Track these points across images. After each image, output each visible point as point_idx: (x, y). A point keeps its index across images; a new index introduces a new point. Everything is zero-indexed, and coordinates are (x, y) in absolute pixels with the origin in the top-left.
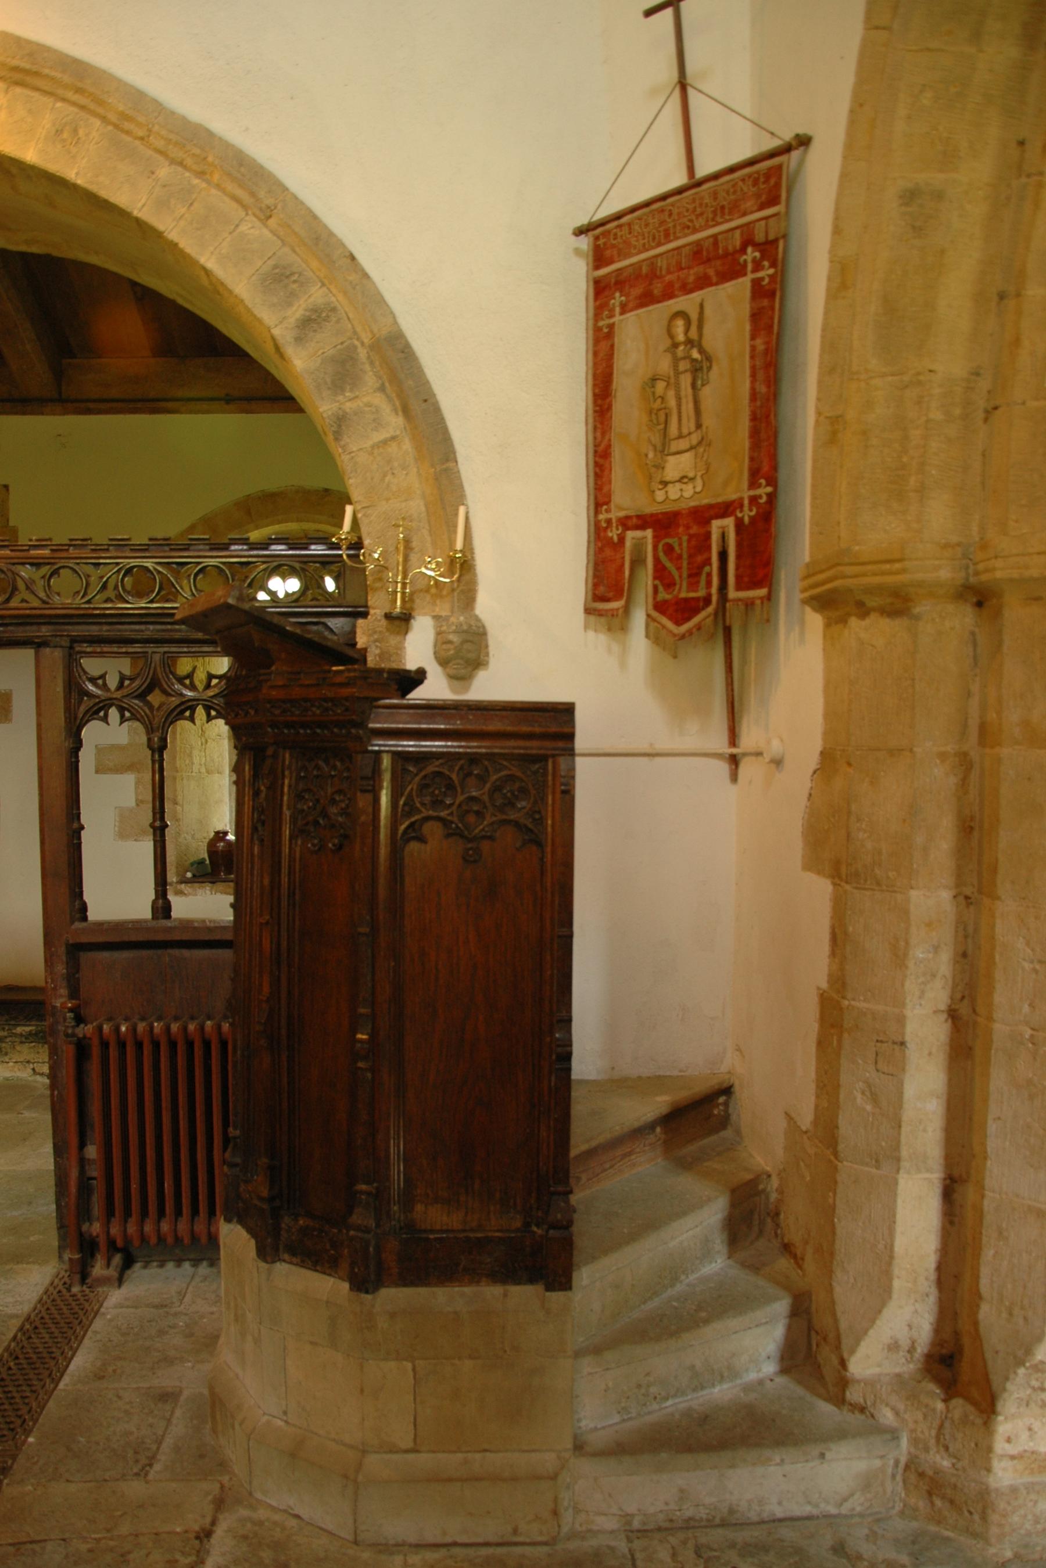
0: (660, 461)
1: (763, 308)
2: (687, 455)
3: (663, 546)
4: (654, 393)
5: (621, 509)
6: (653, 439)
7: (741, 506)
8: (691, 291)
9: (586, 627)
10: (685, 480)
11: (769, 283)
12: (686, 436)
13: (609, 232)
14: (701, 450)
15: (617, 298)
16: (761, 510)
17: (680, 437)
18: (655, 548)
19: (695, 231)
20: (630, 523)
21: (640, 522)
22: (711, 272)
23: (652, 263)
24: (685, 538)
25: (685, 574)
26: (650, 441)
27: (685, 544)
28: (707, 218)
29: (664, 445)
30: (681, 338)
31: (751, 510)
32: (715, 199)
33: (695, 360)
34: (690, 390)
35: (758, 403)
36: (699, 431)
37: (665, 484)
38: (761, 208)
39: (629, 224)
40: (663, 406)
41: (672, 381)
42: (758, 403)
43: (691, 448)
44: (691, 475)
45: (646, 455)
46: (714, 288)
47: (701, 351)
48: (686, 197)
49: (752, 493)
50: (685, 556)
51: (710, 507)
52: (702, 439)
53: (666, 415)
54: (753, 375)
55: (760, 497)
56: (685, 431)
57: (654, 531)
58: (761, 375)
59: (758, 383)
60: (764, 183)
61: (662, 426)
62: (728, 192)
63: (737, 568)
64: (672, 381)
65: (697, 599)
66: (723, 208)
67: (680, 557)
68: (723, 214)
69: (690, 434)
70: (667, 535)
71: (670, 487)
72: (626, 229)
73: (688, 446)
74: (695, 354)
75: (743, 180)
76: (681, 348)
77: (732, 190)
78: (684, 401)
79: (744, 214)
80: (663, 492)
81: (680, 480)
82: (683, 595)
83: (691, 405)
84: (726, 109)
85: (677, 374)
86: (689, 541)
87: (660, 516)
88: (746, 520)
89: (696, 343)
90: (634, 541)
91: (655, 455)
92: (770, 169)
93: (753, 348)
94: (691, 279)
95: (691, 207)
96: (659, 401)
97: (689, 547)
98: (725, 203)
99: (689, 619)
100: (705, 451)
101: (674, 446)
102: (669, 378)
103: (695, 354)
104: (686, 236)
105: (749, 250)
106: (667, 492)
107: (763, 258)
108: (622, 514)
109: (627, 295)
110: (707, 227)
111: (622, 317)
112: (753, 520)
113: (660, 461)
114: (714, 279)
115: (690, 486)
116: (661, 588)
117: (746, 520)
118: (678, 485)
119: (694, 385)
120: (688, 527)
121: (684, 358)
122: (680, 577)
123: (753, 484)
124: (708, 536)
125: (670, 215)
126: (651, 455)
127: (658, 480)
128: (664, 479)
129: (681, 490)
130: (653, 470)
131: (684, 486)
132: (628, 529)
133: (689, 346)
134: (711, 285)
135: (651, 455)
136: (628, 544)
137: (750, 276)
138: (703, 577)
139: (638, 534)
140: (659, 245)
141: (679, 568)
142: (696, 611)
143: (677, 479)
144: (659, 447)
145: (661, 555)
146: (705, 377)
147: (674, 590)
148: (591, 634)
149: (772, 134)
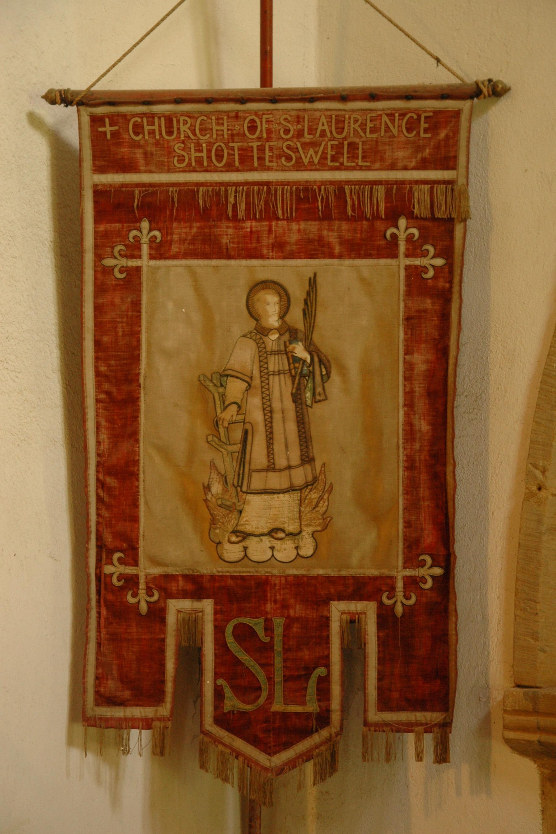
0: (235, 500)
1: (425, 311)
2: (285, 498)
3: (235, 627)
4: (223, 396)
5: (154, 561)
6: (219, 463)
7: (392, 589)
8: (292, 256)
9: (70, 742)
10: (281, 535)
11: (434, 278)
12: (281, 470)
13: (125, 117)
14: (314, 496)
15: (145, 232)
16: (424, 600)
17: (271, 468)
18: (219, 630)
19: (299, 166)
20: (173, 587)
21: (189, 587)
22: (332, 237)
23: (218, 194)
24: (279, 622)
25: (278, 677)
26: (213, 466)
27: (279, 631)
28: (324, 153)
29: (240, 476)
30: (273, 321)
31: (408, 598)
32: (340, 130)
33: (296, 360)
34: (290, 405)
35: (417, 446)
36: (308, 467)
37: (245, 536)
38: (423, 165)
39: (169, 119)
40: (240, 417)
41: (257, 382)
42: (417, 446)
43: (291, 489)
44: (291, 528)
45: (207, 488)
46: (335, 261)
47: (311, 348)
48: (287, 111)
49: (409, 572)
50: (278, 647)
51: (330, 580)
52: (315, 479)
53: (246, 433)
54: (410, 404)
55: (423, 580)
56: (281, 462)
57: (216, 604)
58: (421, 405)
59: (417, 416)
60: (426, 131)
61: (237, 448)
62: (363, 126)
63: (381, 678)
64: (257, 382)
65: (308, 716)
66: (353, 146)
67: (269, 647)
68: (353, 156)
69: (289, 467)
70: (241, 613)
71: (252, 543)
72: (160, 125)
73: (285, 485)
74: (300, 351)
75: (391, 116)
76: (274, 336)
77: (369, 125)
78: (277, 417)
79: (392, 167)
80: (239, 547)
81: (272, 533)
82: (277, 707)
83: (292, 426)
84: (377, 13)
85: (265, 374)
86: (287, 627)
87: (230, 582)
88: (399, 610)
89: (301, 335)
90: (181, 615)
91: (225, 490)
92: (437, 113)
93: (409, 367)
94: (294, 237)
95: (293, 128)
96: (234, 408)
97: (286, 636)
98: (357, 140)
99: (287, 745)
100: (321, 498)
101: (257, 481)
102: (251, 378)
103: (300, 351)
104: (283, 169)
105: (402, 222)
106: (245, 548)
107: (424, 238)
108: (156, 571)
109: (167, 232)
110: (322, 166)
111: (153, 263)
112: (409, 611)
113: (235, 500)
114: (337, 250)
115: (289, 544)
116: (228, 692)
117: (399, 610)
118: (267, 541)
119: (297, 398)
120: (285, 606)
121: (279, 352)
122: (270, 679)
123: (410, 561)
124: (325, 622)
125: (253, 128)
126: (216, 488)
127: (230, 528)
128: (240, 528)
129: (272, 548)
130: (220, 512)
131: (277, 544)
132: (172, 597)
133: (286, 337)
134: (332, 256)
135: (216, 488)
136: (171, 619)
137: (404, 261)
138: (312, 684)
139: (186, 604)
140: (230, 167)
141: (267, 666)
142: (306, 733)
143: (266, 531)
144: (231, 477)
145: (230, 640)
146: (319, 390)
147: (258, 697)
148: (76, 753)
149: (438, 60)
